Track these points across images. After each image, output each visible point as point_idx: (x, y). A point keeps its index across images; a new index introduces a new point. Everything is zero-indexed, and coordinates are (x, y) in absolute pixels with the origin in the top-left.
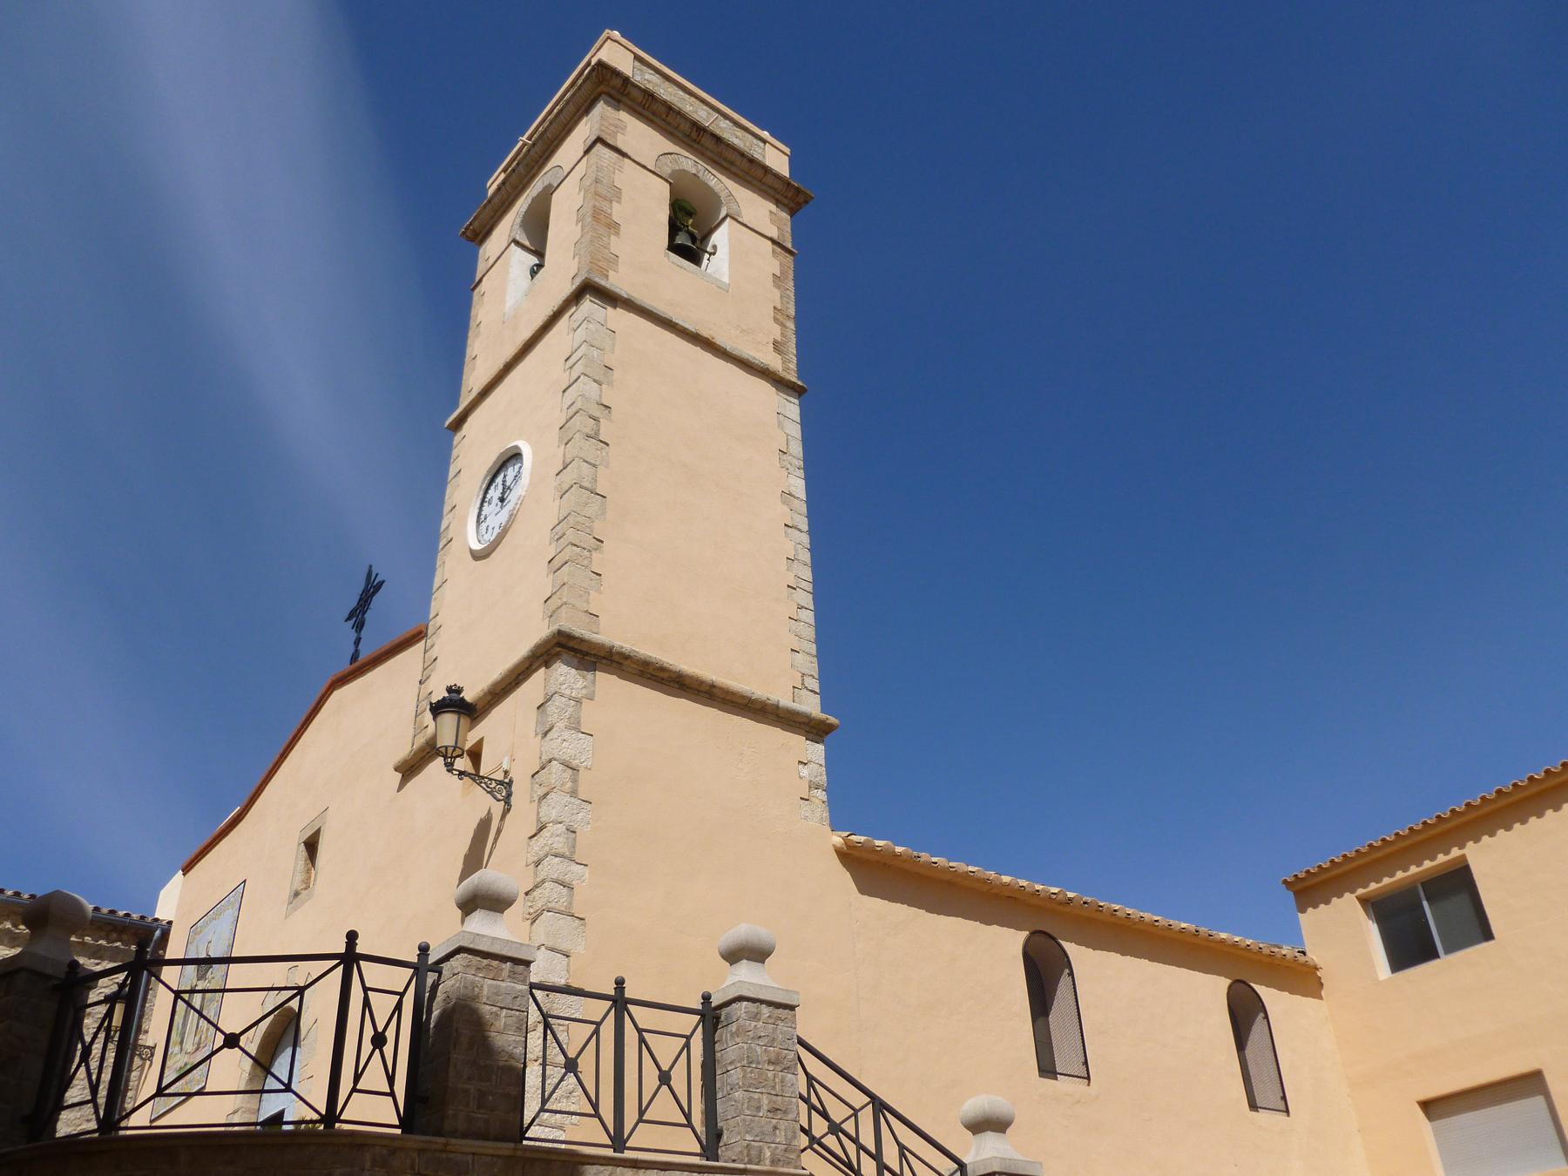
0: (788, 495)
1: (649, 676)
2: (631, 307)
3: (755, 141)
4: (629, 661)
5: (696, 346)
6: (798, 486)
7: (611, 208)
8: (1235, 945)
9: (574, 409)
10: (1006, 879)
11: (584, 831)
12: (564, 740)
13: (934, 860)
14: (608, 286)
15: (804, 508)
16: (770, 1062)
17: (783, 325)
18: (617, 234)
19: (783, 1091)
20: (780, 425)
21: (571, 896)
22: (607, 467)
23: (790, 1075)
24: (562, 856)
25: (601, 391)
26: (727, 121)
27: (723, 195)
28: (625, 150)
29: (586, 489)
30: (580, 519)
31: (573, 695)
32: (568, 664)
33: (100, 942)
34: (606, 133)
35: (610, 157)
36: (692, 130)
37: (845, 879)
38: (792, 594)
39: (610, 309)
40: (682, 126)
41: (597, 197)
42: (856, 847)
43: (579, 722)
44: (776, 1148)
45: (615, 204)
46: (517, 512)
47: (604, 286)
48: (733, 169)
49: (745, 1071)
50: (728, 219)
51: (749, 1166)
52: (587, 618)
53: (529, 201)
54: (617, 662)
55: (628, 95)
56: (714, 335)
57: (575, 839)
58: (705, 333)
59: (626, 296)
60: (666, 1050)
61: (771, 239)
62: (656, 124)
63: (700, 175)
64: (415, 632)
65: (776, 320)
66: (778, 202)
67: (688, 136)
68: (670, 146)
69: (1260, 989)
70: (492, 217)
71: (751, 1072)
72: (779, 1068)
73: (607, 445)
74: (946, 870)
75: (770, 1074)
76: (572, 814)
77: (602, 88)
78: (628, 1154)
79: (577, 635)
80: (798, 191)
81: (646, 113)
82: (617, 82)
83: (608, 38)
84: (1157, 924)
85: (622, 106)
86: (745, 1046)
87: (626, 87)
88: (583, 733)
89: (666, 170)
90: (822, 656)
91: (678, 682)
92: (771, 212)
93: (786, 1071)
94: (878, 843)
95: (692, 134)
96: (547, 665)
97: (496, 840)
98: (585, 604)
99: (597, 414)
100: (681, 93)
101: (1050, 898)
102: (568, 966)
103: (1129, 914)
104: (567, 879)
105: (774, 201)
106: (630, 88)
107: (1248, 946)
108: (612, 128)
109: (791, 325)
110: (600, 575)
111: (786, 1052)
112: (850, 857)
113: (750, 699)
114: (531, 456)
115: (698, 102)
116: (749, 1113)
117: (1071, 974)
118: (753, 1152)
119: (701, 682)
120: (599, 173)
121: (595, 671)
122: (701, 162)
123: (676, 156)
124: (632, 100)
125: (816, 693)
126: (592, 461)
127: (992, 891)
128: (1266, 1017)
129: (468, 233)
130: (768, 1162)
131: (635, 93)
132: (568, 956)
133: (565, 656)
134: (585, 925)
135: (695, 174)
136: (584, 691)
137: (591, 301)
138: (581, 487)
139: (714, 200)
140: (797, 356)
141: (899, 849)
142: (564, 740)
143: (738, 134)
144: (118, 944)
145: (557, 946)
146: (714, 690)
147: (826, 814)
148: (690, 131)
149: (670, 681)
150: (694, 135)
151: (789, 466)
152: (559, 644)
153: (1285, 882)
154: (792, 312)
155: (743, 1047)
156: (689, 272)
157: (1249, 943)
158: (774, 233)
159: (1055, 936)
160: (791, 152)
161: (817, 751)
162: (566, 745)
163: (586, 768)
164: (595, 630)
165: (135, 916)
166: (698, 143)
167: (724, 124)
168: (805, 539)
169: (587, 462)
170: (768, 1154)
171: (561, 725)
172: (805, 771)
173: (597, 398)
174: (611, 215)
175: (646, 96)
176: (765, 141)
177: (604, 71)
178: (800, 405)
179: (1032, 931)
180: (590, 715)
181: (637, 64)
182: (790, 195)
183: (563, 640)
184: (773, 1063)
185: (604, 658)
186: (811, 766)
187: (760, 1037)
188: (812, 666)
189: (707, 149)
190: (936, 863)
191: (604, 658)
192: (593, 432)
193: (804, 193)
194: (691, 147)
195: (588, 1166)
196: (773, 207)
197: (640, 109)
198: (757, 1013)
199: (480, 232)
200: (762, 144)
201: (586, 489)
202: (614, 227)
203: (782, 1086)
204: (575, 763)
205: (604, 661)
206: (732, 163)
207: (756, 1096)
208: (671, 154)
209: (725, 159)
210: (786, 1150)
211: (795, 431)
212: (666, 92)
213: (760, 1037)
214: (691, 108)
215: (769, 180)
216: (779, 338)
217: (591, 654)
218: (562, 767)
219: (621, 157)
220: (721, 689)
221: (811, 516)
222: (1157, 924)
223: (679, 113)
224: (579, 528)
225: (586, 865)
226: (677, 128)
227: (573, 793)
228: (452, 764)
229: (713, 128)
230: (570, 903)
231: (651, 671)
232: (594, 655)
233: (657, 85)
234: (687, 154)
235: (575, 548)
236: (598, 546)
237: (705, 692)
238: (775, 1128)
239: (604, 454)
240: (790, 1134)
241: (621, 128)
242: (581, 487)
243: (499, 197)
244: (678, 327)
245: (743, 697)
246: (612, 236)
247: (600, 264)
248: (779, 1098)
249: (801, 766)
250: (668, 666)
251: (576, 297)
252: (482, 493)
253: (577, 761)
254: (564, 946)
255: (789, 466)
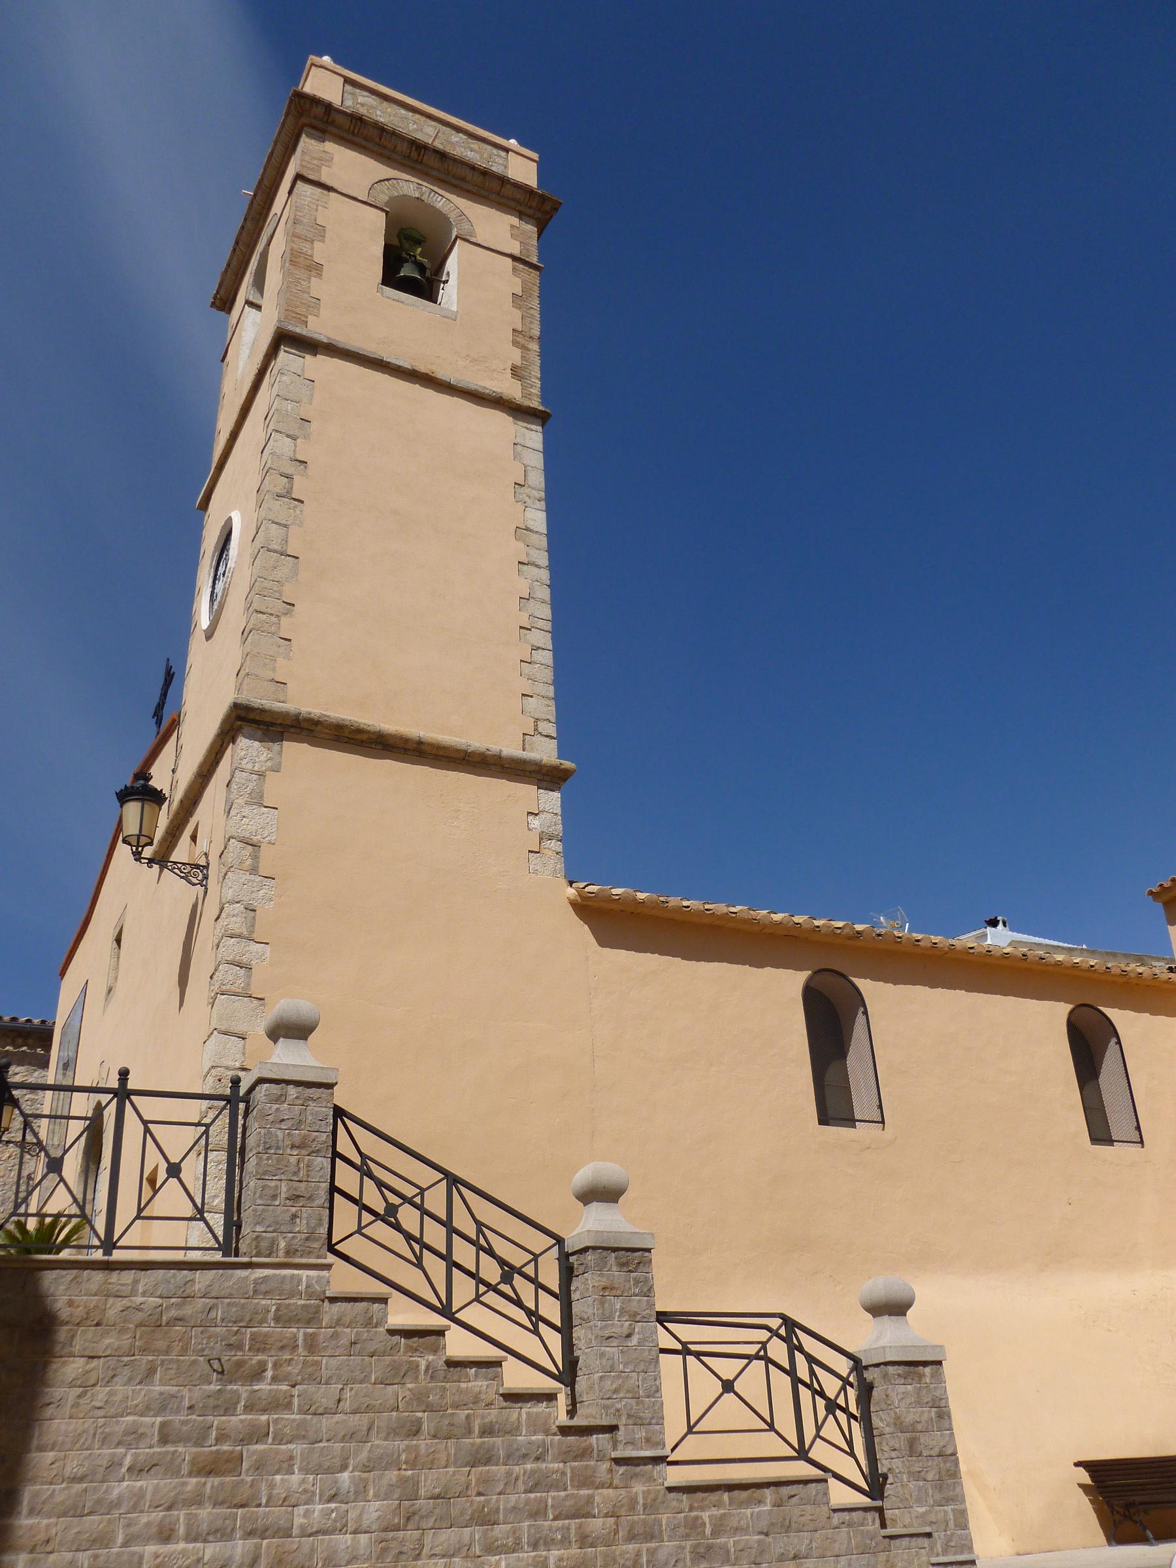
0: (523, 531)
1: (346, 740)
2: (333, 351)
3: (495, 151)
4: (319, 727)
5: (415, 384)
6: (538, 519)
7: (313, 249)
8: (1075, 966)
9: (265, 471)
10: (778, 917)
11: (266, 911)
12: (244, 817)
13: (685, 903)
14: (309, 335)
15: (544, 542)
16: (293, 1147)
17: (524, 348)
18: (320, 275)
19: (308, 1176)
20: (517, 456)
21: (249, 977)
22: (301, 526)
23: (319, 1159)
24: (239, 936)
25: (296, 446)
26: (461, 135)
27: (452, 216)
28: (330, 183)
29: (275, 551)
30: (266, 584)
31: (256, 768)
32: (250, 737)
33: (7, 1048)
34: (308, 168)
35: (312, 193)
36: (411, 150)
37: (583, 931)
38: (526, 635)
39: (308, 357)
40: (399, 148)
41: (295, 239)
42: (590, 897)
43: (262, 797)
44: (293, 1238)
45: (317, 244)
46: (229, 585)
47: (300, 334)
48: (465, 186)
49: (261, 1158)
50: (458, 241)
51: (254, 1259)
52: (273, 686)
53: (258, 256)
54: (308, 729)
55: (333, 123)
56: (434, 368)
57: (254, 918)
58: (423, 368)
59: (326, 341)
60: (176, 1142)
61: (514, 258)
62: (369, 150)
63: (425, 198)
64: (170, 721)
65: (515, 343)
66: (521, 215)
67: (408, 157)
68: (385, 171)
69: (1110, 1012)
70: (235, 282)
71: (268, 1159)
72: (304, 1152)
73: (302, 502)
74: (700, 914)
75: (293, 1160)
76: (252, 892)
77: (304, 120)
78: (117, 1255)
79: (256, 706)
80: (543, 199)
81: (357, 140)
82: (319, 111)
83: (312, 64)
84: (972, 951)
85: (327, 136)
86: (263, 1131)
87: (329, 115)
88: (266, 807)
89: (382, 198)
90: (560, 699)
91: (380, 743)
92: (512, 226)
93: (314, 1155)
94: (614, 891)
95: (412, 154)
96: (234, 740)
97: (198, 928)
98: (271, 672)
99: (289, 471)
100: (403, 111)
101: (833, 932)
102: (244, 1048)
103: (935, 944)
104: (245, 959)
105: (517, 213)
106: (334, 115)
107: (1092, 966)
108: (315, 162)
109: (535, 347)
110: (290, 640)
111: (315, 1133)
112: (584, 908)
113: (465, 752)
114: (240, 525)
115: (423, 119)
116: (262, 1202)
117: (865, 1013)
118: (264, 1244)
119: (405, 740)
120: (298, 213)
121: (282, 741)
122: (425, 184)
123: (395, 181)
124: (339, 127)
125: (552, 738)
126: (283, 522)
127: (765, 931)
128: (1119, 1043)
129: (218, 303)
130: (281, 1253)
131: (340, 120)
132: (244, 1039)
133: (246, 730)
134: (263, 1005)
135: (418, 198)
136: (269, 764)
137: (285, 351)
138: (269, 550)
139: (443, 221)
140: (541, 379)
141: (641, 896)
142: (244, 817)
143: (473, 146)
144: (24, 1048)
145: (231, 1030)
146: (423, 747)
147: (560, 866)
148: (408, 151)
149: (371, 743)
150: (414, 154)
151: (527, 499)
152: (239, 718)
153: (1151, 893)
154: (536, 331)
155: (260, 1133)
156: (408, 304)
157: (1093, 964)
158: (515, 249)
159: (844, 973)
160: (539, 157)
161: (552, 800)
162: (252, 822)
163: (270, 843)
164: (282, 699)
165: (36, 1021)
166: (421, 163)
167: (457, 138)
168: (545, 575)
169: (276, 523)
170: (282, 1244)
171: (241, 801)
172: (535, 823)
173: (291, 454)
174: (312, 256)
175: (354, 121)
176: (507, 150)
177: (302, 101)
178: (543, 433)
179: (816, 969)
180: (273, 788)
181: (348, 88)
182: (534, 204)
183: (243, 714)
184: (298, 1147)
185: (292, 726)
186: (542, 816)
187: (283, 1120)
188: (548, 710)
189: (432, 168)
190: (688, 907)
191: (292, 726)
192: (285, 491)
193: (549, 199)
194: (413, 168)
195: (46, 1272)
196: (515, 221)
197: (350, 137)
198: (281, 1095)
199: (228, 299)
200: (503, 154)
201: (275, 551)
202: (316, 269)
203: (308, 1171)
204: (255, 839)
205: (292, 730)
206: (463, 179)
207: (273, 1184)
208: (388, 180)
209: (454, 176)
210: (307, 1239)
211: (536, 460)
212: (385, 114)
213: (283, 1120)
214: (415, 126)
215: (508, 191)
216: (518, 362)
217: (276, 724)
218: (241, 845)
219: (326, 192)
220: (431, 745)
221: (551, 550)
222: (972, 951)
223: (394, 134)
224: (265, 594)
225: (268, 944)
226: (394, 150)
227: (254, 870)
228: (140, 853)
229: (438, 145)
230: (248, 984)
231: (347, 734)
232: (280, 724)
233: (372, 107)
234: (408, 177)
235: (260, 615)
236: (288, 610)
237: (414, 750)
238: (294, 1216)
239: (298, 512)
240: (313, 1223)
241: (328, 160)
242: (269, 550)
243: (235, 259)
244: (391, 366)
245: (458, 751)
246: (313, 279)
247: (298, 310)
248: (303, 1185)
249: (531, 818)
250: (365, 727)
251: (272, 353)
252: (212, 571)
253: (259, 837)
254: (239, 1029)
255: (527, 499)
